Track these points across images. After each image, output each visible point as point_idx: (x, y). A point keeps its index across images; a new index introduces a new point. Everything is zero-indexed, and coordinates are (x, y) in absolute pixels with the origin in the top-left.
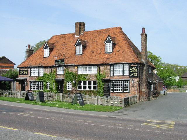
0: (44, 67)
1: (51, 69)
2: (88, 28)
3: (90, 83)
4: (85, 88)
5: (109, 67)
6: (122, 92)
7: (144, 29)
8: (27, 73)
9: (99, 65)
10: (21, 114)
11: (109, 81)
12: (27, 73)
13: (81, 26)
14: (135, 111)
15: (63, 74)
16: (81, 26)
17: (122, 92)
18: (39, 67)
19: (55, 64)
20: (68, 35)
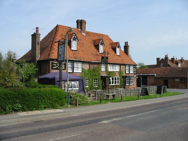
0: (83, 62)
1: (120, 67)
2: (89, 28)
3: (115, 78)
4: (113, 83)
5: (125, 67)
6: (128, 84)
7: (37, 28)
8: (64, 68)
9: (120, 65)
10: (11, 139)
11: (126, 77)
12: (64, 68)
13: (81, 23)
14: (112, 102)
15: (105, 70)
16: (81, 23)
17: (128, 84)
18: (129, 65)
19: (101, 61)
20: (63, 27)
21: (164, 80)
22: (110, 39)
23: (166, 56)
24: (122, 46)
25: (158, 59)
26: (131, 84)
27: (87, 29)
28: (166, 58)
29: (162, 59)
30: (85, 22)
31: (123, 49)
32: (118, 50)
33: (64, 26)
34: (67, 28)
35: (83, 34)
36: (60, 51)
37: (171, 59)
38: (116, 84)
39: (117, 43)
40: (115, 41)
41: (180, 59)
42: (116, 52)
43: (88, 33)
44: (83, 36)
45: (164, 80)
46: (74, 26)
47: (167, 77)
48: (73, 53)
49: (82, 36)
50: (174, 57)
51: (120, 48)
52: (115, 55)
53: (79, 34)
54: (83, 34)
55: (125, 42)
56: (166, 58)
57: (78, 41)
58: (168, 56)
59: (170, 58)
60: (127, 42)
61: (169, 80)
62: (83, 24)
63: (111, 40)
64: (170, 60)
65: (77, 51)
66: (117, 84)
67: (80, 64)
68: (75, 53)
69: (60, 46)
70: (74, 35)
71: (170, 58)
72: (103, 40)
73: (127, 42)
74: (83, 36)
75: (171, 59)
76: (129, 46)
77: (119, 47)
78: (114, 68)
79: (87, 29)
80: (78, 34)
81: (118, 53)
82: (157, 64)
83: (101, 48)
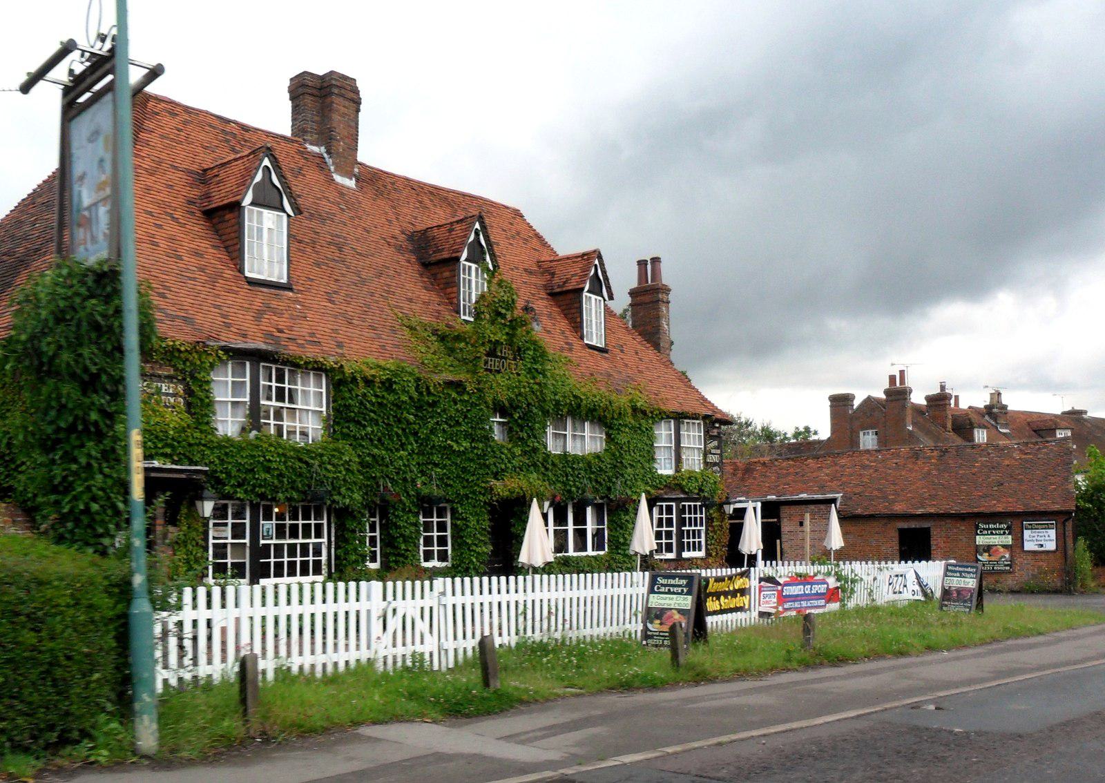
2: (379, 147)
13: (325, 101)
16: (325, 101)
21: (902, 532)
22: (539, 237)
23: (892, 379)
24: (623, 279)
25: (840, 403)
26: (686, 555)
27: (370, 152)
28: (898, 393)
29: (869, 401)
30: (356, 92)
31: (621, 302)
32: (592, 306)
33: (187, 110)
34: (217, 123)
35: (338, 178)
36: (82, 178)
37: (928, 398)
38: (584, 554)
39: (591, 258)
40: (566, 245)
41: (980, 400)
42: (577, 325)
43: (373, 180)
44: (341, 194)
45: (902, 532)
46: (275, 116)
47: (920, 511)
48: (258, 303)
49: (332, 195)
50: (943, 388)
51: (611, 297)
52: (572, 339)
53: (312, 175)
54: (338, 178)
55: (642, 264)
56: (898, 393)
57: (297, 209)
58: (909, 383)
59: (918, 398)
60: (656, 260)
61: (934, 532)
62: (339, 103)
63: (545, 244)
64: (917, 409)
65: (287, 287)
66: (590, 552)
67: (312, 389)
68: (274, 304)
69: (82, 127)
70: (266, 162)
71: (918, 398)
72: (487, 221)
73: (656, 260)
74: (341, 191)
75: (928, 398)
76: (667, 290)
77: (600, 285)
78: (569, 433)
79: (370, 152)
80: (299, 172)
81: (595, 333)
82: (833, 431)
83: (472, 283)
